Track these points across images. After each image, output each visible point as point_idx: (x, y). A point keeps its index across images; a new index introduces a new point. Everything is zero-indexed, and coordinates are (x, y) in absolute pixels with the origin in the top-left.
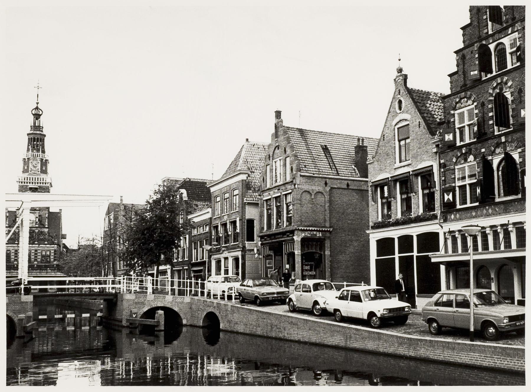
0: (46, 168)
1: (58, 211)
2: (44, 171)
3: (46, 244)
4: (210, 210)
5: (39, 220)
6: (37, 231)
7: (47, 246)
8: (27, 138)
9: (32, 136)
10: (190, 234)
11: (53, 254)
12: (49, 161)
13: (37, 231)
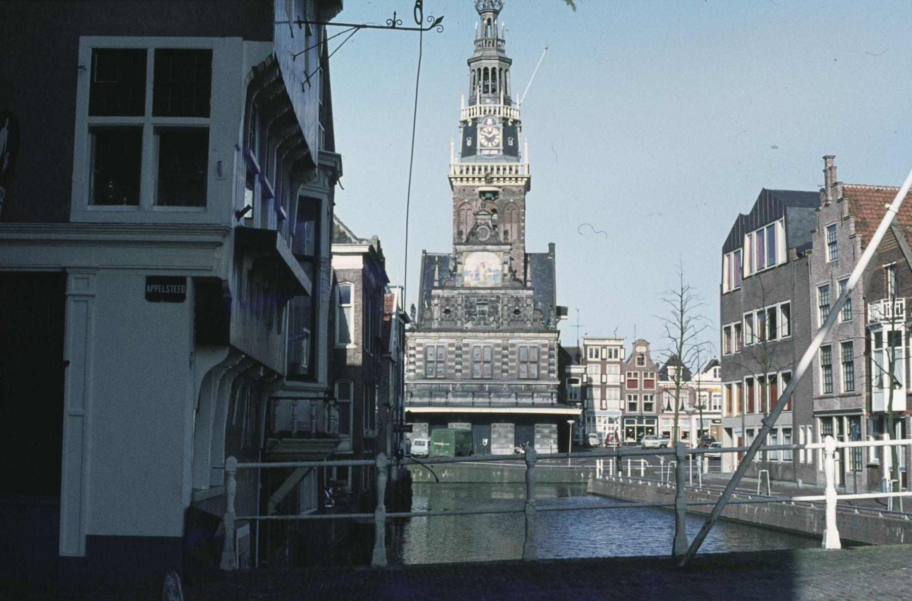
1: (546, 251)
2: (511, 151)
5: (510, 269)
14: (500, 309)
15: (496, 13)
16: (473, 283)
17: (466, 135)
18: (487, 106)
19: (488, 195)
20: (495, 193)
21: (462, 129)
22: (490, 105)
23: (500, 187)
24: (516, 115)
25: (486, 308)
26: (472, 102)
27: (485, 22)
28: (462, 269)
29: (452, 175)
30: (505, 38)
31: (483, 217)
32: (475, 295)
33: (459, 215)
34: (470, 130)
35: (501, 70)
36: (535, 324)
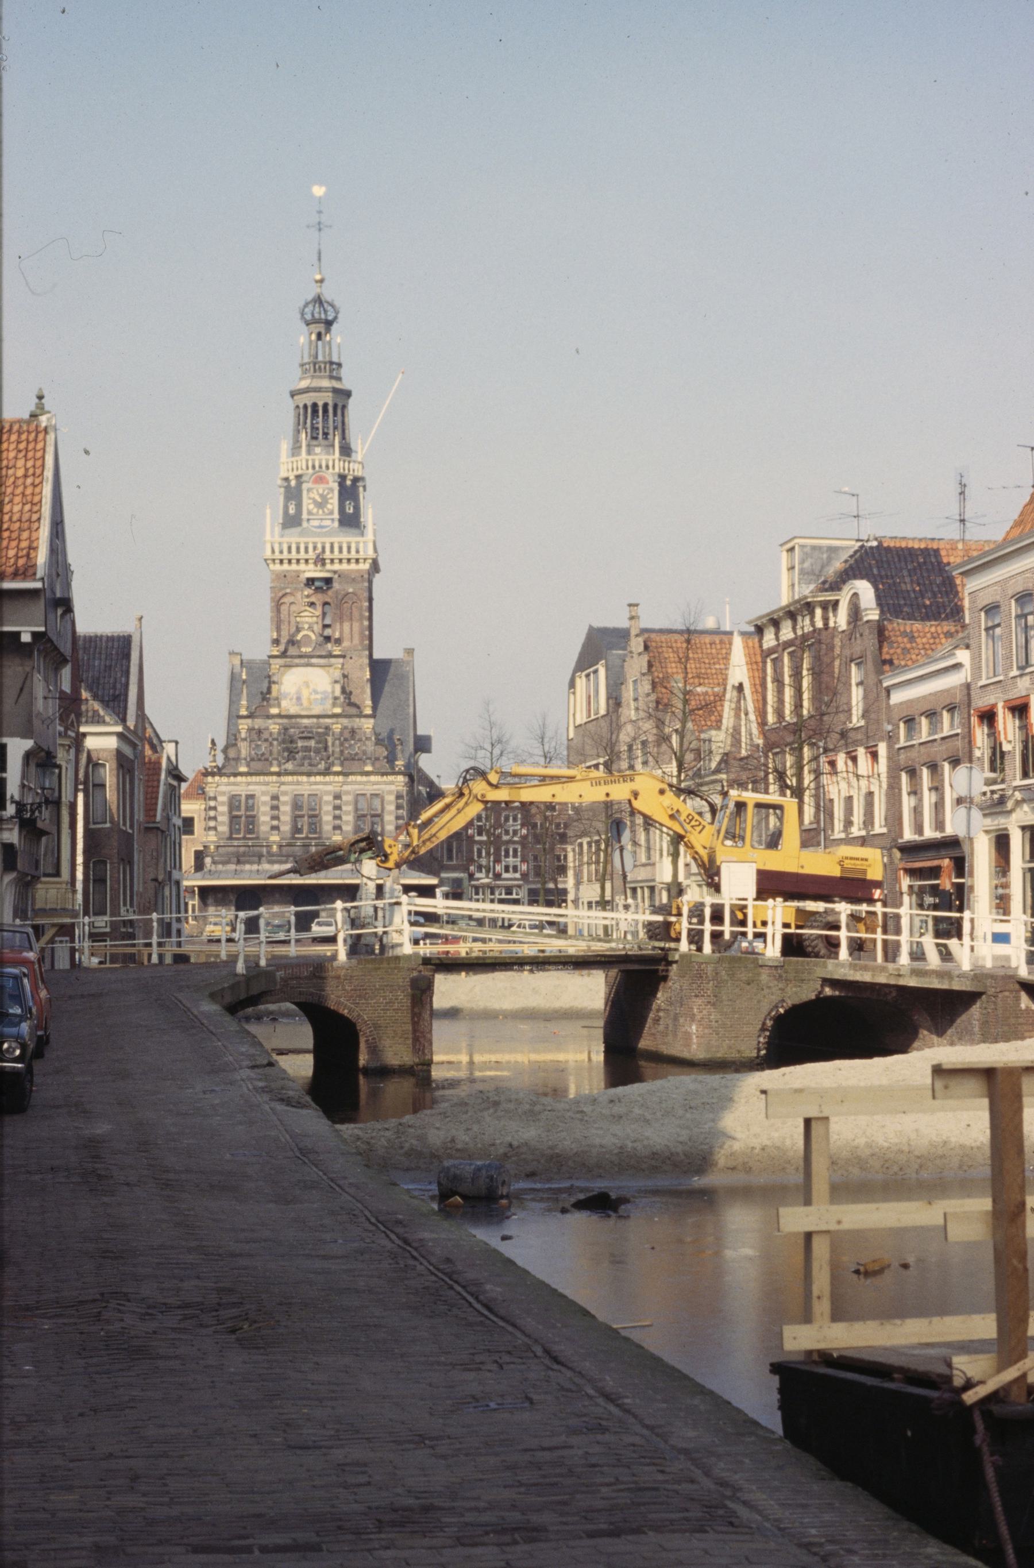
0: (357, 508)
2: (351, 521)
3: (367, 774)
4: (963, 656)
5: (343, 691)
6: (337, 728)
7: (373, 778)
8: (289, 405)
9: (308, 399)
10: (891, 738)
11: (392, 807)
12: (368, 483)
13: (337, 728)
14: (330, 744)
15: (329, 324)
16: (293, 710)
17: (288, 498)
18: (316, 457)
19: (317, 584)
20: (328, 581)
21: (282, 490)
22: (320, 455)
23: (335, 572)
24: (355, 469)
25: (312, 743)
26: (296, 449)
27: (314, 337)
28: (279, 690)
29: (268, 554)
30: (342, 361)
31: (307, 619)
32: (296, 726)
33: (278, 611)
34: (293, 492)
35: (335, 406)
36: (378, 764)
